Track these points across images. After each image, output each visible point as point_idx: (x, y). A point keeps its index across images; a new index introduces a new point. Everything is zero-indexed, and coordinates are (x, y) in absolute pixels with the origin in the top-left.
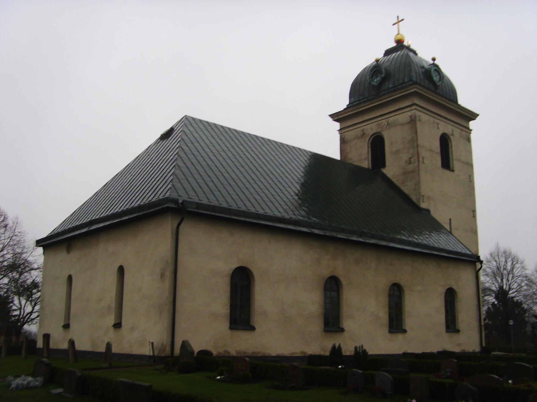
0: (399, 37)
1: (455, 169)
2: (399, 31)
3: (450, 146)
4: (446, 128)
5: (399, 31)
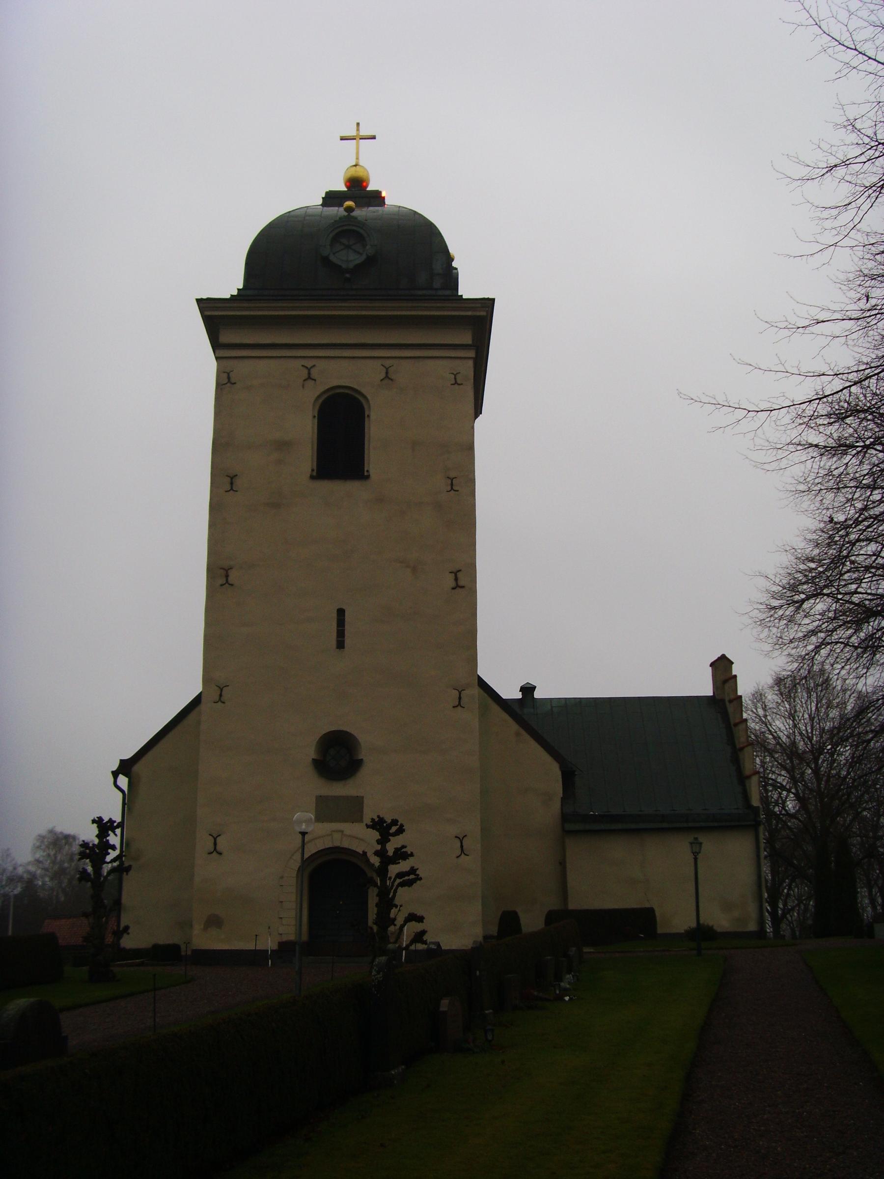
0: (353, 172)
1: (372, 472)
2: (357, 158)
3: (367, 413)
4: (338, 373)
5: (357, 158)
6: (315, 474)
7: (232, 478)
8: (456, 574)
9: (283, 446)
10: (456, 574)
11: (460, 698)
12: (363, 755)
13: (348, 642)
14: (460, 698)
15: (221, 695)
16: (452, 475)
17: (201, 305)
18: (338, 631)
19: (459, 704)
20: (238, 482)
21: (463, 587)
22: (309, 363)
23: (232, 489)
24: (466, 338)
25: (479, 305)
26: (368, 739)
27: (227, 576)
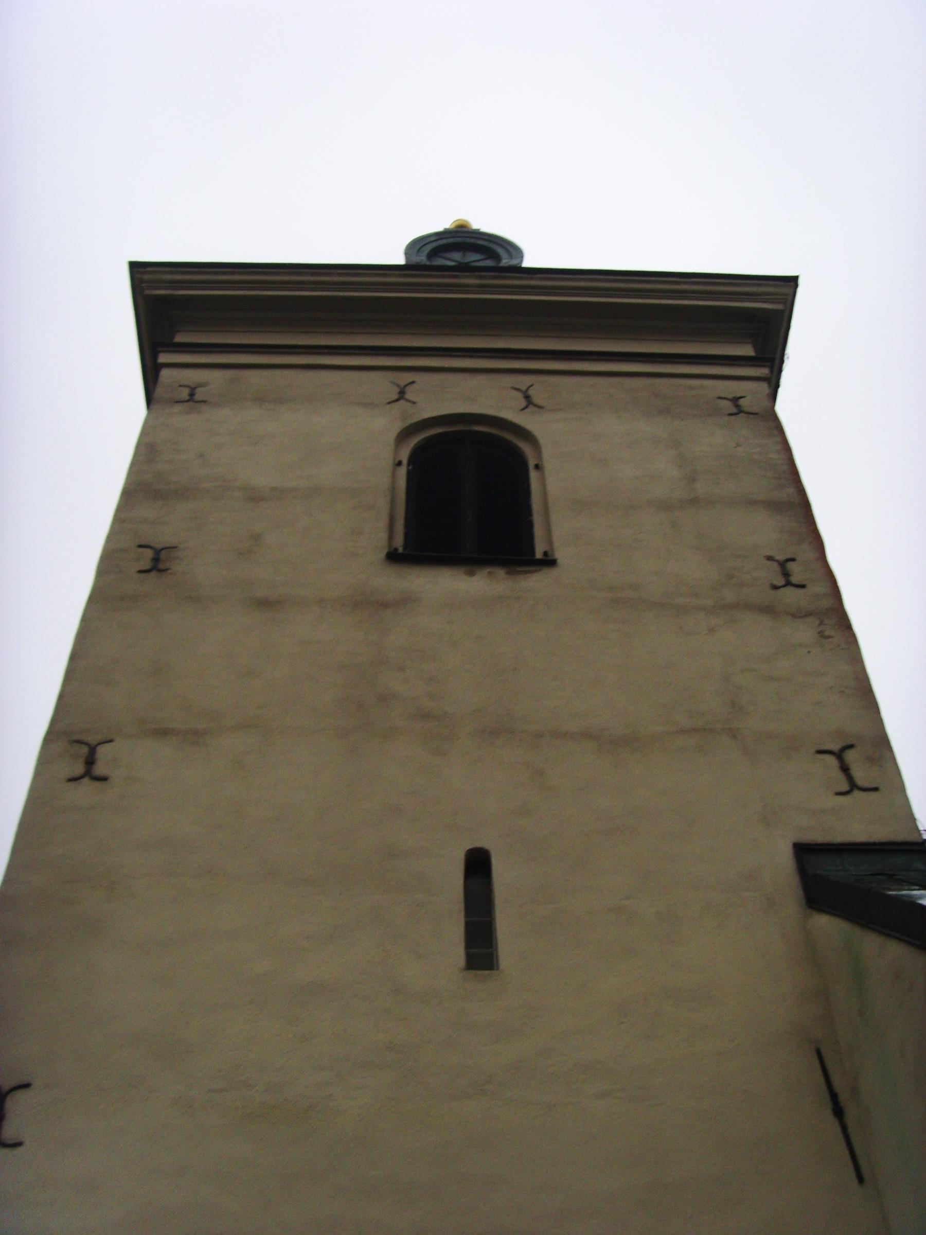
1: (560, 554)
6: (399, 541)
24: (764, 371)
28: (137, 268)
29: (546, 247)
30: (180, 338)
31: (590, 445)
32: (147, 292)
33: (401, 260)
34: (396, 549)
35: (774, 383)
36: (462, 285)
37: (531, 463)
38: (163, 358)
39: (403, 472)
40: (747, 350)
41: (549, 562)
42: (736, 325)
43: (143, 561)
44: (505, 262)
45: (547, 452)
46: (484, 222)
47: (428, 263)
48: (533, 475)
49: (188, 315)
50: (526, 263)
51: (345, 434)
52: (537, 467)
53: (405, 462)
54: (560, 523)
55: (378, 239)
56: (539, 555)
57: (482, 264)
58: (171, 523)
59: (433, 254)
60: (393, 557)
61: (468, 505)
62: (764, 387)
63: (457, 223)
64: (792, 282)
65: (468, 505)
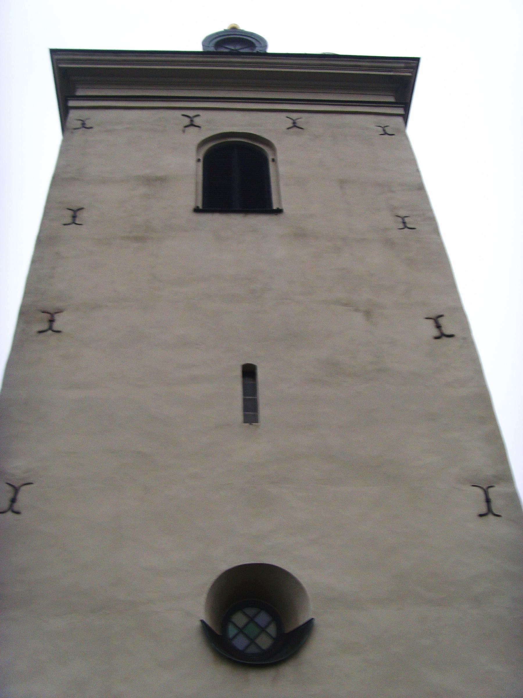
1: (284, 206)
6: (200, 206)
7: (75, 213)
8: (436, 320)
9: (155, 182)
10: (436, 320)
11: (488, 501)
12: (311, 610)
13: (263, 412)
14: (488, 501)
15: (13, 501)
16: (402, 213)
17: (56, 57)
18: (245, 402)
19: (490, 511)
20: (82, 216)
21: (451, 336)
22: (191, 113)
23: (50, 328)
24: (401, 111)
25: (402, 65)
26: (317, 574)
27: (52, 321)
28: (54, 52)
29: (280, 42)
30: (80, 92)
31: (302, 151)
32: (61, 66)
33: (200, 49)
34: (198, 207)
35: (405, 117)
36: (235, 63)
37: (270, 158)
38: (71, 103)
39: (201, 164)
40: (392, 99)
41: (279, 211)
42: (387, 84)
43: (66, 212)
44: (258, 49)
45: (280, 157)
46: (247, 26)
47: (215, 50)
48: (271, 165)
49: (85, 79)
50: (269, 50)
51: (171, 147)
52: (273, 160)
53: (202, 160)
54: (284, 189)
55: (188, 37)
56: (275, 207)
57: (242, 51)
58: (75, 195)
59: (219, 44)
60: (197, 210)
61: (237, 181)
62: (400, 120)
63: (232, 26)
64: (416, 61)
65: (237, 181)
